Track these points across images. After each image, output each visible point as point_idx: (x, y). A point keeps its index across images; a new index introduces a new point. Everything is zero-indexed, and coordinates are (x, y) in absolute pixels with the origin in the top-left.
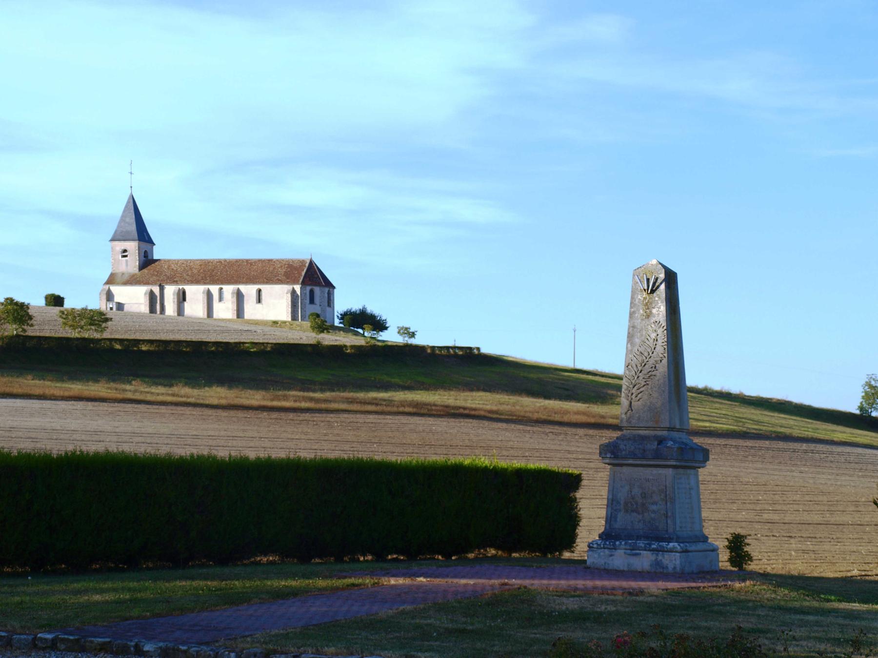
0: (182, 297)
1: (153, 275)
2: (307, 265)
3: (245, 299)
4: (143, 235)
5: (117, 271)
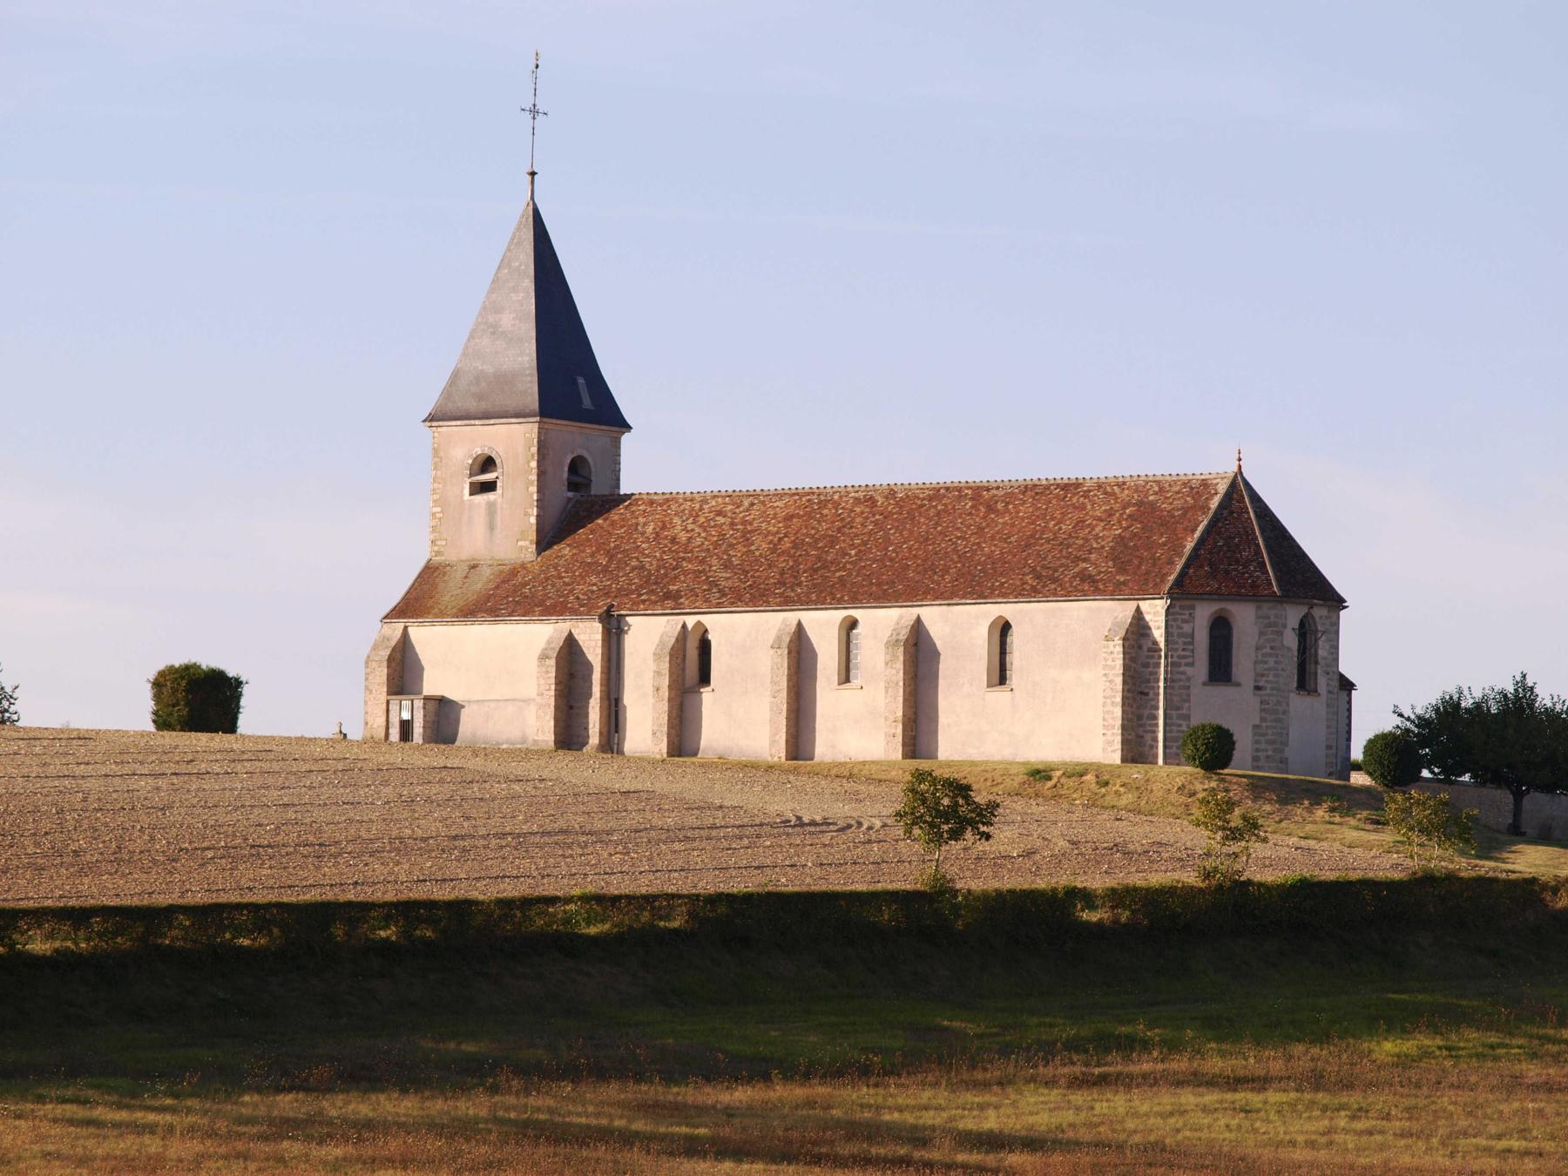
0: (693, 666)
1: (589, 568)
2: (1214, 503)
3: (945, 667)
4: (570, 384)
5: (450, 556)
